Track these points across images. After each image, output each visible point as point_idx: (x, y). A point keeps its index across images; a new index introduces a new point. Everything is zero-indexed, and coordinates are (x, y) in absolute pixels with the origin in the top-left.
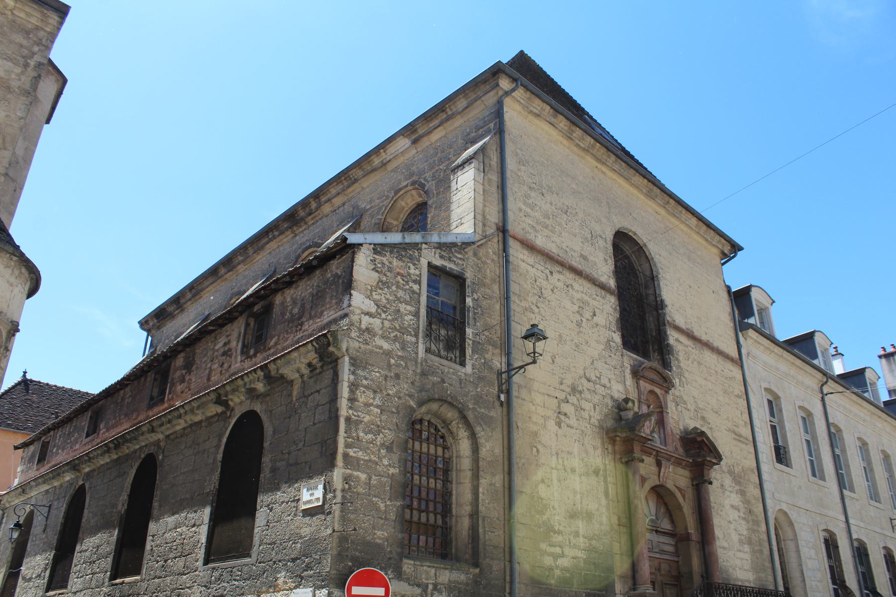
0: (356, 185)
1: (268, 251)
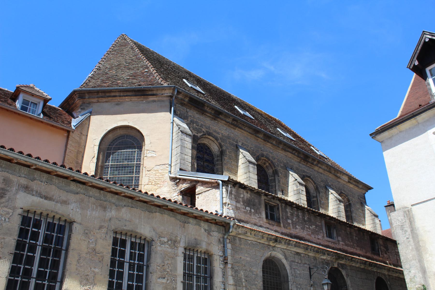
0: (329, 173)
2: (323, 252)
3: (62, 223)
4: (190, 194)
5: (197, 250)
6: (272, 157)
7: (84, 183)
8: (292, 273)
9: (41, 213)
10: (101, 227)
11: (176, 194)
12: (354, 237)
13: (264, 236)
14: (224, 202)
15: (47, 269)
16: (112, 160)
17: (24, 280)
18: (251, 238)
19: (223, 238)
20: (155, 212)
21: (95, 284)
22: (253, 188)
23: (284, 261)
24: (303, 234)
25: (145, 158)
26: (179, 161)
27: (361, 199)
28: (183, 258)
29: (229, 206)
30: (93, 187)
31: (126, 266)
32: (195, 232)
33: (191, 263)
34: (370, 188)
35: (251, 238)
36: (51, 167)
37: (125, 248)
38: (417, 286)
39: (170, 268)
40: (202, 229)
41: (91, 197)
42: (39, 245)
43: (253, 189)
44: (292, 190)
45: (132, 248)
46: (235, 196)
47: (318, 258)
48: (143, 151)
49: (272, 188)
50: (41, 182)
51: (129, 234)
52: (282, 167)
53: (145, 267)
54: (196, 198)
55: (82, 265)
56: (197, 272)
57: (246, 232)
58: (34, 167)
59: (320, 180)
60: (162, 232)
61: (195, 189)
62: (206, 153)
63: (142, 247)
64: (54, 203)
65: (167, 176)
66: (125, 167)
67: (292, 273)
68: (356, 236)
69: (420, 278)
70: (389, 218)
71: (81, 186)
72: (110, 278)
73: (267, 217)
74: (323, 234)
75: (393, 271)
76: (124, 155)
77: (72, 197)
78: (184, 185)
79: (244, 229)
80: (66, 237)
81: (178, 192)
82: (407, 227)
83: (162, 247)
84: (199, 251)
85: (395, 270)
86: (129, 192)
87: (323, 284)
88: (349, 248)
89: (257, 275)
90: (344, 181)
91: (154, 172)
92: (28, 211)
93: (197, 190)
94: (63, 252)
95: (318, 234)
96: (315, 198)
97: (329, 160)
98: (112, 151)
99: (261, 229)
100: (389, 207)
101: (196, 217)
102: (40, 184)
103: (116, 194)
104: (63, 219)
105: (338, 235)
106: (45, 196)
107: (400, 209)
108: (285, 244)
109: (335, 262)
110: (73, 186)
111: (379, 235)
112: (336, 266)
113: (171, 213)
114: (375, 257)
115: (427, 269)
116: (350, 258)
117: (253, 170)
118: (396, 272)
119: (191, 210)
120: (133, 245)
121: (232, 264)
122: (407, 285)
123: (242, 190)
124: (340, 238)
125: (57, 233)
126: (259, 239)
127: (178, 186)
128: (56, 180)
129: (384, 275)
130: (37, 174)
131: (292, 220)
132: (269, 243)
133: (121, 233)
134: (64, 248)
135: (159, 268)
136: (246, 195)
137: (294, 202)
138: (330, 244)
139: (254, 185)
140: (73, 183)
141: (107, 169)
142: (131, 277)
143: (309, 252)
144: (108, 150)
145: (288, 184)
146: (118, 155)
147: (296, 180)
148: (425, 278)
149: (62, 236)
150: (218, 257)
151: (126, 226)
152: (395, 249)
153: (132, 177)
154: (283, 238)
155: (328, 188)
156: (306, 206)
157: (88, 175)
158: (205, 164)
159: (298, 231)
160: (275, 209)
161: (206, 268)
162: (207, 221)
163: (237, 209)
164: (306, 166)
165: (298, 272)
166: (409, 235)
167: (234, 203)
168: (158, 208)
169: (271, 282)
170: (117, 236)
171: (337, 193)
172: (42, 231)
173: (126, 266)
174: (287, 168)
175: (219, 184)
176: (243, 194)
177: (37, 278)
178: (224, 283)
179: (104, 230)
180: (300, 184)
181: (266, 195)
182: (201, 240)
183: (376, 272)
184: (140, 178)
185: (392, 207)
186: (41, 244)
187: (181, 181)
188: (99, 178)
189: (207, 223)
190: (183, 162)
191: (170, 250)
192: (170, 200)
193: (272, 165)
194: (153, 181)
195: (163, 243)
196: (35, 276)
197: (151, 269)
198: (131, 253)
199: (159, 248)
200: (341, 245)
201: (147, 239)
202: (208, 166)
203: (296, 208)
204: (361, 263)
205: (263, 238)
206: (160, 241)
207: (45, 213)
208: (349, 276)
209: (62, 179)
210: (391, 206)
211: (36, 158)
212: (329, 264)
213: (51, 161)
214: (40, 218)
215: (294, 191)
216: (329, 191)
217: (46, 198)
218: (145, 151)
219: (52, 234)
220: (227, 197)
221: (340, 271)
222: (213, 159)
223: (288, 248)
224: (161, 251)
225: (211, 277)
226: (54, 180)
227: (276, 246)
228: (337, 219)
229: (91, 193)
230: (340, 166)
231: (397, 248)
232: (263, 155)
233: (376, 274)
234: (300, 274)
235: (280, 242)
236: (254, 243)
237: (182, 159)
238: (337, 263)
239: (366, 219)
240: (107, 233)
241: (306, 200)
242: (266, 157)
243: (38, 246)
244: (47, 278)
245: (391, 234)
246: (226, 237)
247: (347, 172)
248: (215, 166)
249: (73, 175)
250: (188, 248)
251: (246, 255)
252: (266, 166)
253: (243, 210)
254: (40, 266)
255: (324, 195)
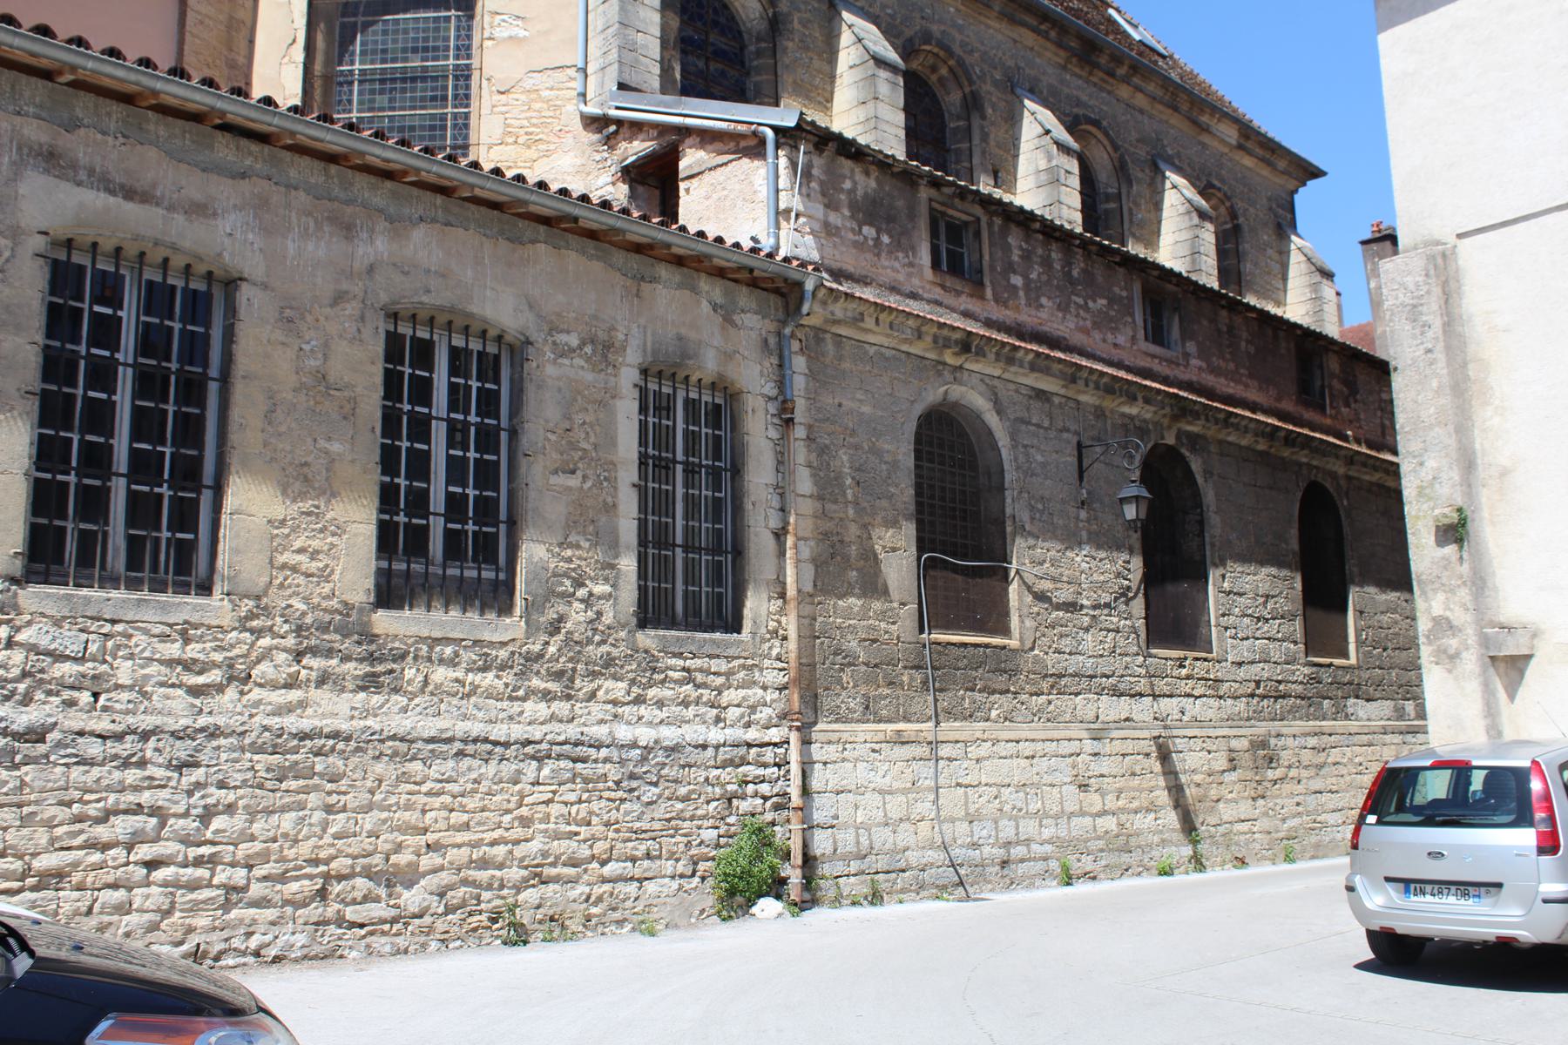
1: (1015, 36)
2: (1130, 393)
3: (198, 285)
4: (657, 179)
5: (687, 378)
6: (963, 45)
7: (263, 138)
8: (1016, 459)
9: (118, 250)
10: (339, 298)
11: (606, 178)
12: (1243, 344)
13: (924, 329)
14: (782, 206)
15: (163, 444)
16: (363, 53)
17: (87, 481)
18: (878, 338)
19: (779, 334)
20: (533, 242)
21: (334, 495)
22: (887, 156)
23: (992, 419)
24: (1063, 327)
25: (487, 43)
26: (614, 55)
27: (1281, 211)
28: (636, 405)
29: (802, 220)
30: (300, 150)
31: (439, 432)
32: (677, 312)
33: (664, 422)
34: (1316, 173)
35: (878, 338)
36: (133, 77)
37: (431, 370)
38: (1437, 512)
39: (592, 439)
40: (705, 303)
41: (296, 189)
42: (126, 365)
43: (890, 161)
44: (1032, 169)
45: (454, 371)
46: (822, 183)
47: (1112, 411)
48: (478, 18)
49: (958, 162)
50: (104, 133)
51: (441, 319)
52: (996, 83)
53: (504, 436)
54: (682, 193)
55: (283, 429)
56: (686, 453)
57: (862, 314)
58: (69, 77)
59: (1134, 135)
60: (559, 315)
61: (677, 160)
62: (716, 23)
63: (489, 367)
64: (161, 211)
65: (571, 113)
66: (414, 79)
67: (1016, 459)
68: (1248, 342)
69: (1453, 486)
70: (1373, 285)
71: (255, 147)
72: (384, 473)
73: (936, 265)
74: (1135, 330)
75: (1364, 465)
76: (406, 31)
77: (223, 191)
78: (636, 143)
79: (853, 305)
80: (216, 334)
81: (613, 169)
82: (1432, 314)
83: (561, 365)
84: (694, 379)
85: (1371, 462)
86: (435, 168)
87: (1122, 501)
88: (1222, 380)
89: (895, 464)
90: (1222, 141)
91: (523, 97)
92: (70, 241)
93: (682, 164)
94: (213, 387)
95: (1114, 330)
96: (1112, 198)
97: (1175, 61)
98: (361, 19)
99: (915, 307)
100: (1375, 247)
101: (679, 261)
102: (98, 141)
103: (388, 175)
104: (201, 269)
105: (1186, 335)
106: (122, 187)
107: (1415, 248)
108: (997, 360)
109: (1169, 427)
110: (225, 149)
111: (1331, 341)
112: (1170, 440)
113: (590, 243)
114: (1309, 415)
115: (1479, 455)
116: (1222, 416)
117: (891, 92)
118: (1375, 469)
119: (661, 236)
120: (458, 359)
121: (810, 427)
122: (1406, 509)
123: (847, 164)
124: (1191, 347)
125: (183, 320)
126: (905, 341)
127: (612, 148)
128: (158, 127)
129: (1333, 476)
130: (83, 105)
131: (1026, 277)
132: (941, 354)
133: (414, 316)
134: (214, 372)
135: (553, 437)
136: (862, 182)
137: (1038, 212)
138: (1156, 366)
139: (894, 145)
140: (222, 138)
141: (345, 88)
142: (456, 469)
143: (1079, 392)
144: (343, 15)
145: (1016, 147)
146: (385, 32)
147: (1048, 132)
148: (1470, 486)
149: (201, 330)
150: (761, 401)
151: (429, 291)
152: (1381, 391)
153: (443, 117)
154: (990, 339)
155: (1162, 165)
156: (1079, 230)
157: (277, 106)
158: (713, 66)
159: (1046, 316)
160: (968, 237)
161: (717, 439)
162: (720, 273)
163: (827, 231)
164: (1087, 81)
165: (1039, 458)
166: (1436, 339)
167: (819, 210)
168: (542, 228)
169: (943, 489)
170: (401, 330)
171: (1193, 185)
172: (129, 315)
173: (439, 432)
174: (1016, 86)
175: (762, 142)
176: (852, 178)
177: (134, 475)
178: (781, 491)
179: (352, 308)
180: (1062, 147)
181: (936, 183)
182: (700, 341)
183: (1308, 464)
184: (473, 121)
185: (1388, 244)
186: (130, 361)
187: (625, 130)
188: (319, 118)
189: (720, 282)
190: (628, 57)
191: (589, 377)
192: (584, 198)
193: (959, 72)
194: (522, 131)
195: (564, 352)
196: (123, 469)
197: (525, 442)
198: (453, 389)
199: (550, 370)
200: (1195, 369)
201: (508, 338)
202: (723, 73)
203: (1043, 233)
204: (1256, 435)
205: (919, 337)
206: (554, 343)
207: (131, 250)
208: (1212, 474)
209: (180, 122)
210: (1385, 240)
211: (70, 41)
212: (1148, 432)
213: (132, 55)
214: (117, 267)
215: (1038, 173)
216: (1164, 177)
217: (129, 194)
218: (487, 18)
219: (167, 323)
220: (792, 189)
221: (1183, 457)
222: (743, 48)
223: (1006, 376)
224: (559, 379)
225: (737, 471)
226: (152, 127)
227: (967, 366)
228: (1188, 279)
229: (293, 173)
230: (1214, 87)
231: (1390, 386)
232: (927, 37)
233: (1305, 471)
234: (1044, 465)
235: (980, 353)
236: (888, 353)
237: (627, 48)
238: (1173, 432)
239: (1291, 284)
240: (363, 318)
241: (1079, 206)
242: (940, 45)
243: (121, 368)
244: (166, 476)
245: (1372, 342)
246: (787, 331)
247: (1235, 111)
248: (748, 74)
249: (219, 104)
250: (655, 369)
251: (859, 396)
252: (941, 80)
253: (851, 236)
254: (136, 435)
255: (1147, 193)
